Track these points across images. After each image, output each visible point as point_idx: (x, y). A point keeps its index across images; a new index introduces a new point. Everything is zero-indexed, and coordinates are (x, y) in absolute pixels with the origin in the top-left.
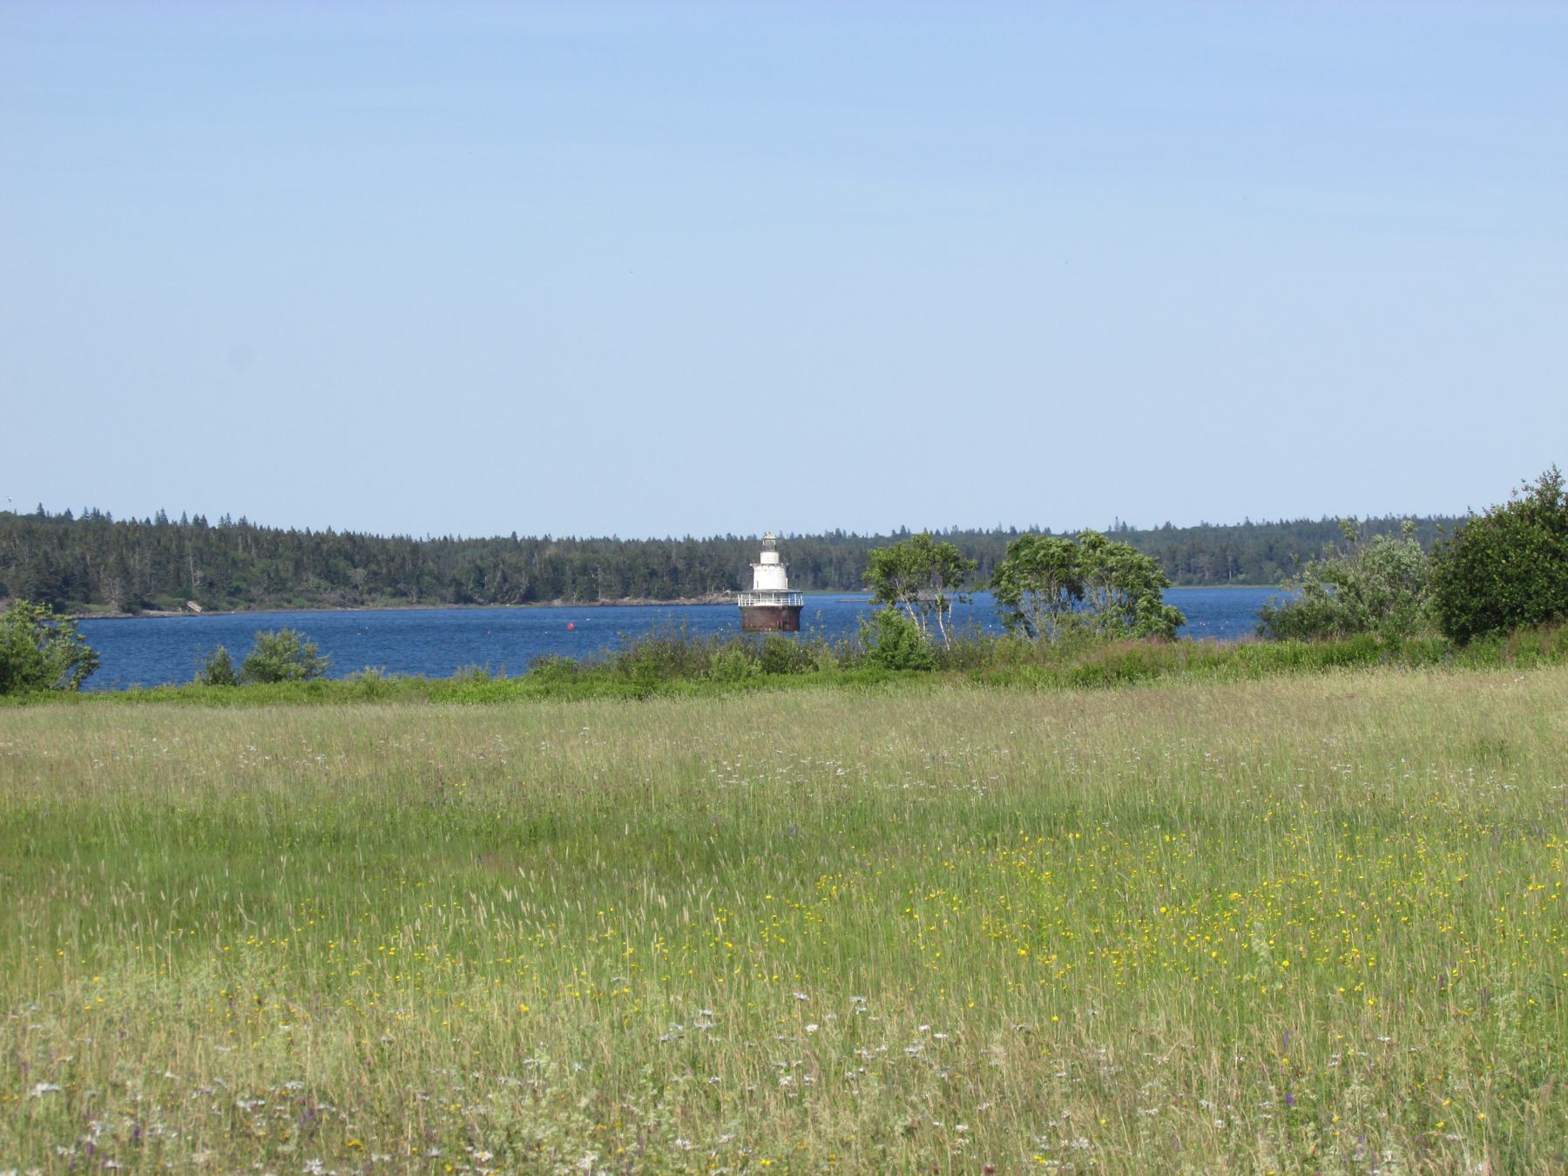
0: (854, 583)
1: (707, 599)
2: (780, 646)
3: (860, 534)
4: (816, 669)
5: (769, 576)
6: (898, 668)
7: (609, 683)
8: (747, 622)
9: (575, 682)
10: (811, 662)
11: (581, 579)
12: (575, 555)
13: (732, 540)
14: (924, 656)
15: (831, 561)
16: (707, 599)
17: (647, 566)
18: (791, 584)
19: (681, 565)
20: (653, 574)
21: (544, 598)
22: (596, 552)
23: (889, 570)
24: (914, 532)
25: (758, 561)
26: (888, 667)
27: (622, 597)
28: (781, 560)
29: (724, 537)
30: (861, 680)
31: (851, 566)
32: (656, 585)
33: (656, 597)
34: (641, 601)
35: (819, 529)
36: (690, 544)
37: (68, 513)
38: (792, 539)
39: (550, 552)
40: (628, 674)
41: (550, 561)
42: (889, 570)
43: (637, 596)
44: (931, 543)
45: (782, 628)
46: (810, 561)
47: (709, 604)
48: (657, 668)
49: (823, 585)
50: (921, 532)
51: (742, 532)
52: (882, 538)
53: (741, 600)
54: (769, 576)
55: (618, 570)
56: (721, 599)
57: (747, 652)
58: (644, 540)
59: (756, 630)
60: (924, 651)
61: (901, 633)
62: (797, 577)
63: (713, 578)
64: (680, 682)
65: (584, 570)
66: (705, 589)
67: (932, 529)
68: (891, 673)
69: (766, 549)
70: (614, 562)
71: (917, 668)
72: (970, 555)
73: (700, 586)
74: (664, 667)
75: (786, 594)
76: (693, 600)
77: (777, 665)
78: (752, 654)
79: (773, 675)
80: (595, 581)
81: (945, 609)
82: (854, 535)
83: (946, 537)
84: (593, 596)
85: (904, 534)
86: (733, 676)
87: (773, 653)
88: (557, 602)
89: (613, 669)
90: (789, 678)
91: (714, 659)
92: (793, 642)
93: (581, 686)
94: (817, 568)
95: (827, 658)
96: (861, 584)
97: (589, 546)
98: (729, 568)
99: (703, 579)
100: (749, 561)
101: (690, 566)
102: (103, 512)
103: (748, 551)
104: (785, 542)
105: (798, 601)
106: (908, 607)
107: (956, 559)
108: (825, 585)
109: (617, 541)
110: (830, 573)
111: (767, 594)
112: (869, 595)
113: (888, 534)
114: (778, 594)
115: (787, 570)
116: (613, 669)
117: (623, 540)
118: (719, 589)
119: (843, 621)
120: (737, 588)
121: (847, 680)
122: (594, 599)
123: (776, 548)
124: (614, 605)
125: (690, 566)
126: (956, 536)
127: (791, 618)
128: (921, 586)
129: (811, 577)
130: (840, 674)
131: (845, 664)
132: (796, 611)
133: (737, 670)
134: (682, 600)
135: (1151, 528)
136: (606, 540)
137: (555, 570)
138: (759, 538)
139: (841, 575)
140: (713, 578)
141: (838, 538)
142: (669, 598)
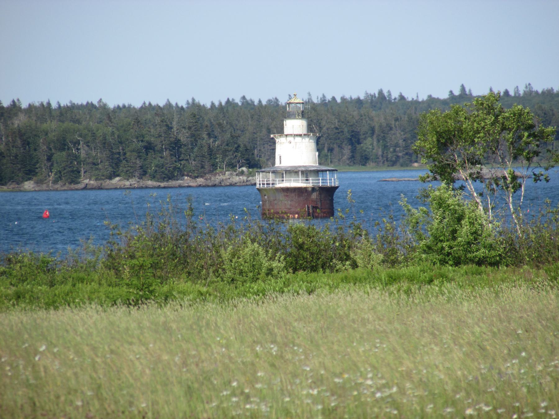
0: (406, 157)
1: (218, 178)
2: (312, 241)
3: (410, 96)
4: (355, 265)
5: (295, 150)
6: (457, 263)
7: (95, 285)
8: (269, 208)
9: (52, 284)
10: (348, 258)
11: (60, 156)
12: (52, 125)
13: (247, 104)
14: (491, 247)
15: (373, 130)
16: (218, 178)
17: (140, 137)
18: (322, 158)
19: (184, 137)
20: (149, 147)
21: (11, 179)
22: (78, 122)
23: (445, 141)
24: (475, 94)
25: (280, 131)
26: (443, 262)
27: (110, 178)
28: (310, 129)
29: (238, 101)
30: (411, 279)
31: (397, 136)
32: (154, 162)
33: (153, 177)
34: (133, 182)
35: (357, 91)
36: (195, 111)
37: (49, 104)
38: (324, 103)
39: (19, 121)
40: (118, 273)
41: (20, 133)
42: (445, 141)
43: (129, 175)
44: (498, 105)
45: (312, 215)
46: (343, 130)
47: (219, 185)
48: (154, 266)
49: (361, 159)
50: (485, 92)
51: (260, 95)
52: (438, 100)
53: (260, 179)
54: (295, 150)
55: (105, 143)
56: (236, 179)
57: (267, 246)
58: (137, 105)
59: (281, 217)
60: (490, 241)
61: (460, 219)
62: (331, 150)
63: (225, 153)
64: (182, 284)
65: (62, 145)
66: (214, 166)
67: (499, 89)
68: (449, 269)
69: (290, 116)
70: (100, 133)
71: (480, 263)
72: (547, 123)
73: (209, 162)
74: (164, 265)
75: (317, 172)
76: (200, 181)
77: (310, 261)
78: (271, 248)
79: (301, 273)
80: (77, 157)
81: (517, 187)
82: (402, 98)
83: (518, 99)
84: (74, 177)
85: (464, 96)
86: (248, 277)
87: (301, 247)
88: (29, 185)
89: (100, 265)
90: (322, 278)
91: (226, 255)
92: (325, 231)
93: (60, 289)
94: (355, 139)
95: (367, 253)
96: (409, 157)
97: (68, 113)
98: (243, 140)
99: (211, 153)
100: (269, 132)
101: (195, 138)
102: (90, 102)
103: (267, 120)
104: (314, 107)
105: (331, 180)
106: (470, 186)
107: (531, 127)
108: (364, 160)
109: (104, 107)
110: (370, 144)
111: (293, 172)
112: (416, 174)
113: (444, 95)
114: (306, 173)
115: (318, 142)
116: (100, 265)
117: (111, 105)
118: (231, 166)
119: (385, 204)
120: (254, 165)
121: (393, 279)
122: (74, 181)
123: (303, 115)
124: (100, 188)
125: (195, 138)
126: (530, 96)
127: (322, 202)
128: (487, 160)
129: (347, 151)
130: (384, 272)
131: (391, 261)
132: (329, 192)
133: (255, 268)
134: (187, 181)
135: (80, 103)
136: (90, 107)
137: (26, 143)
138: (283, 101)
139: (385, 147)
140: (225, 153)
141: (380, 101)
142: (170, 177)
